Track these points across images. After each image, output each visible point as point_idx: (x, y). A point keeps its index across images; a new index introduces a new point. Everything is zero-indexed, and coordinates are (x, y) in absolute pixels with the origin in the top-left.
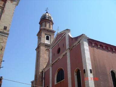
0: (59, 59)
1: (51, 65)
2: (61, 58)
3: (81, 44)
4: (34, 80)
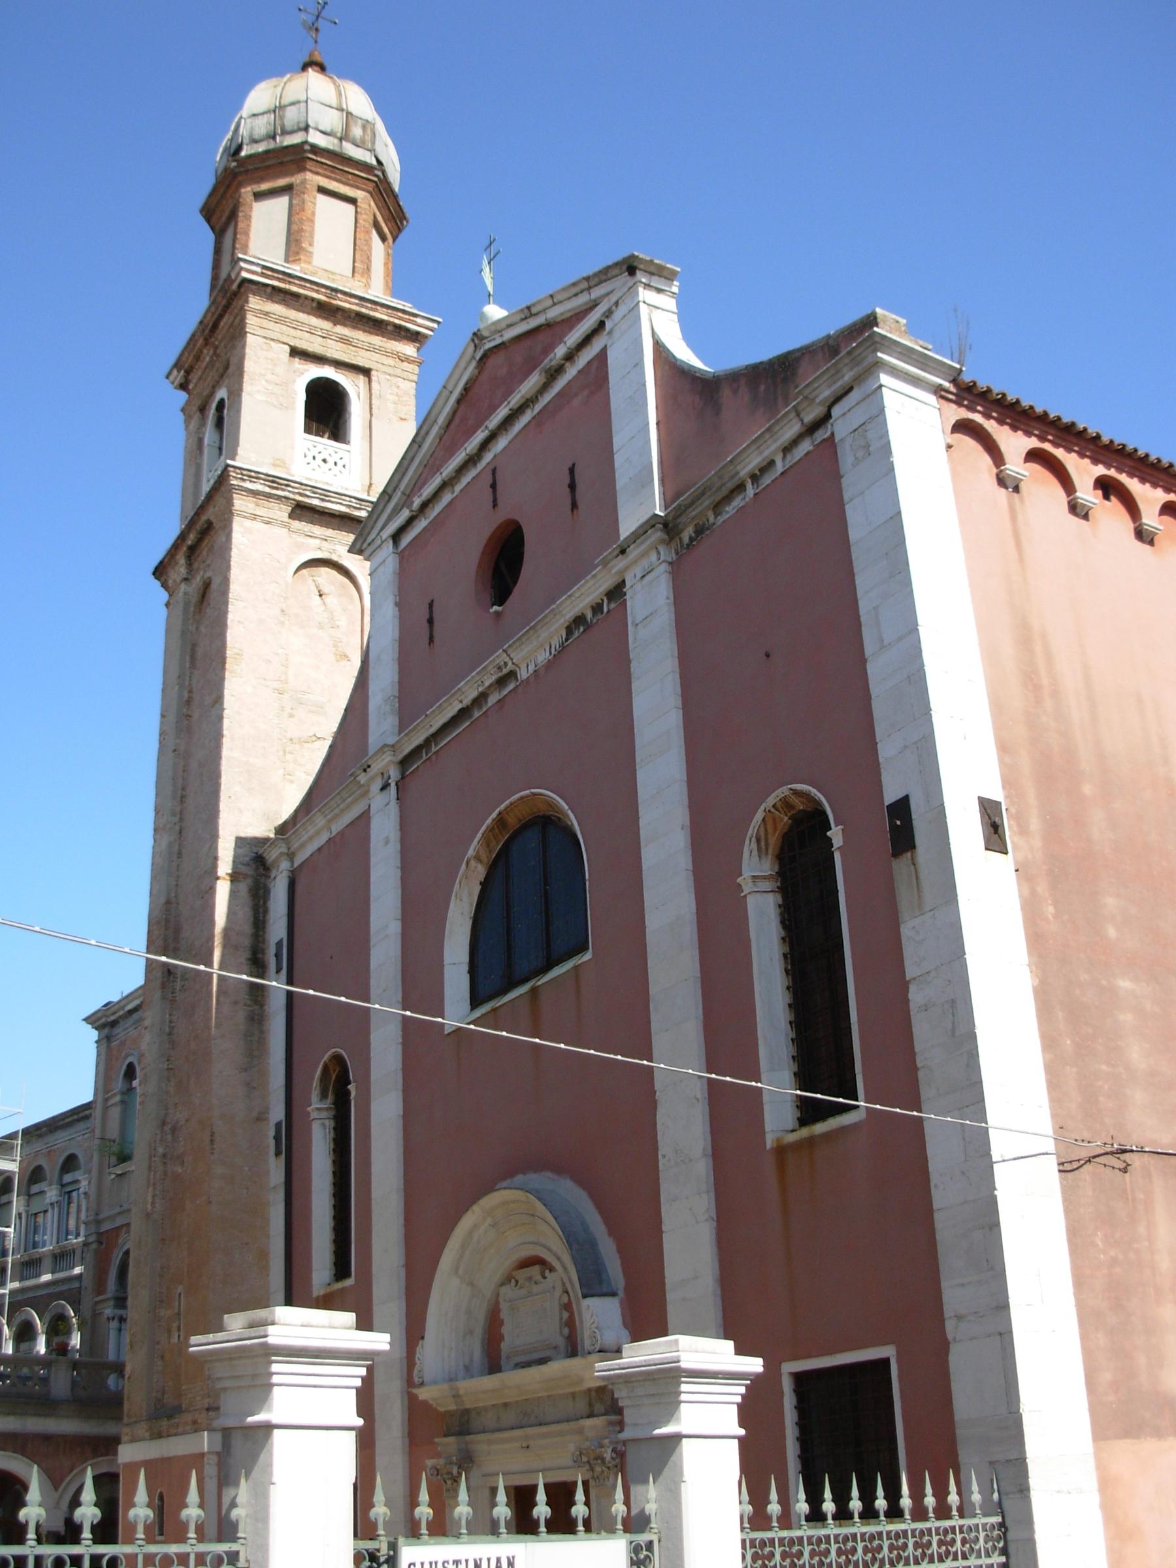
0: (501, 682)
1: (394, 774)
2: (543, 657)
3: (846, 459)
4: (502, 1331)
